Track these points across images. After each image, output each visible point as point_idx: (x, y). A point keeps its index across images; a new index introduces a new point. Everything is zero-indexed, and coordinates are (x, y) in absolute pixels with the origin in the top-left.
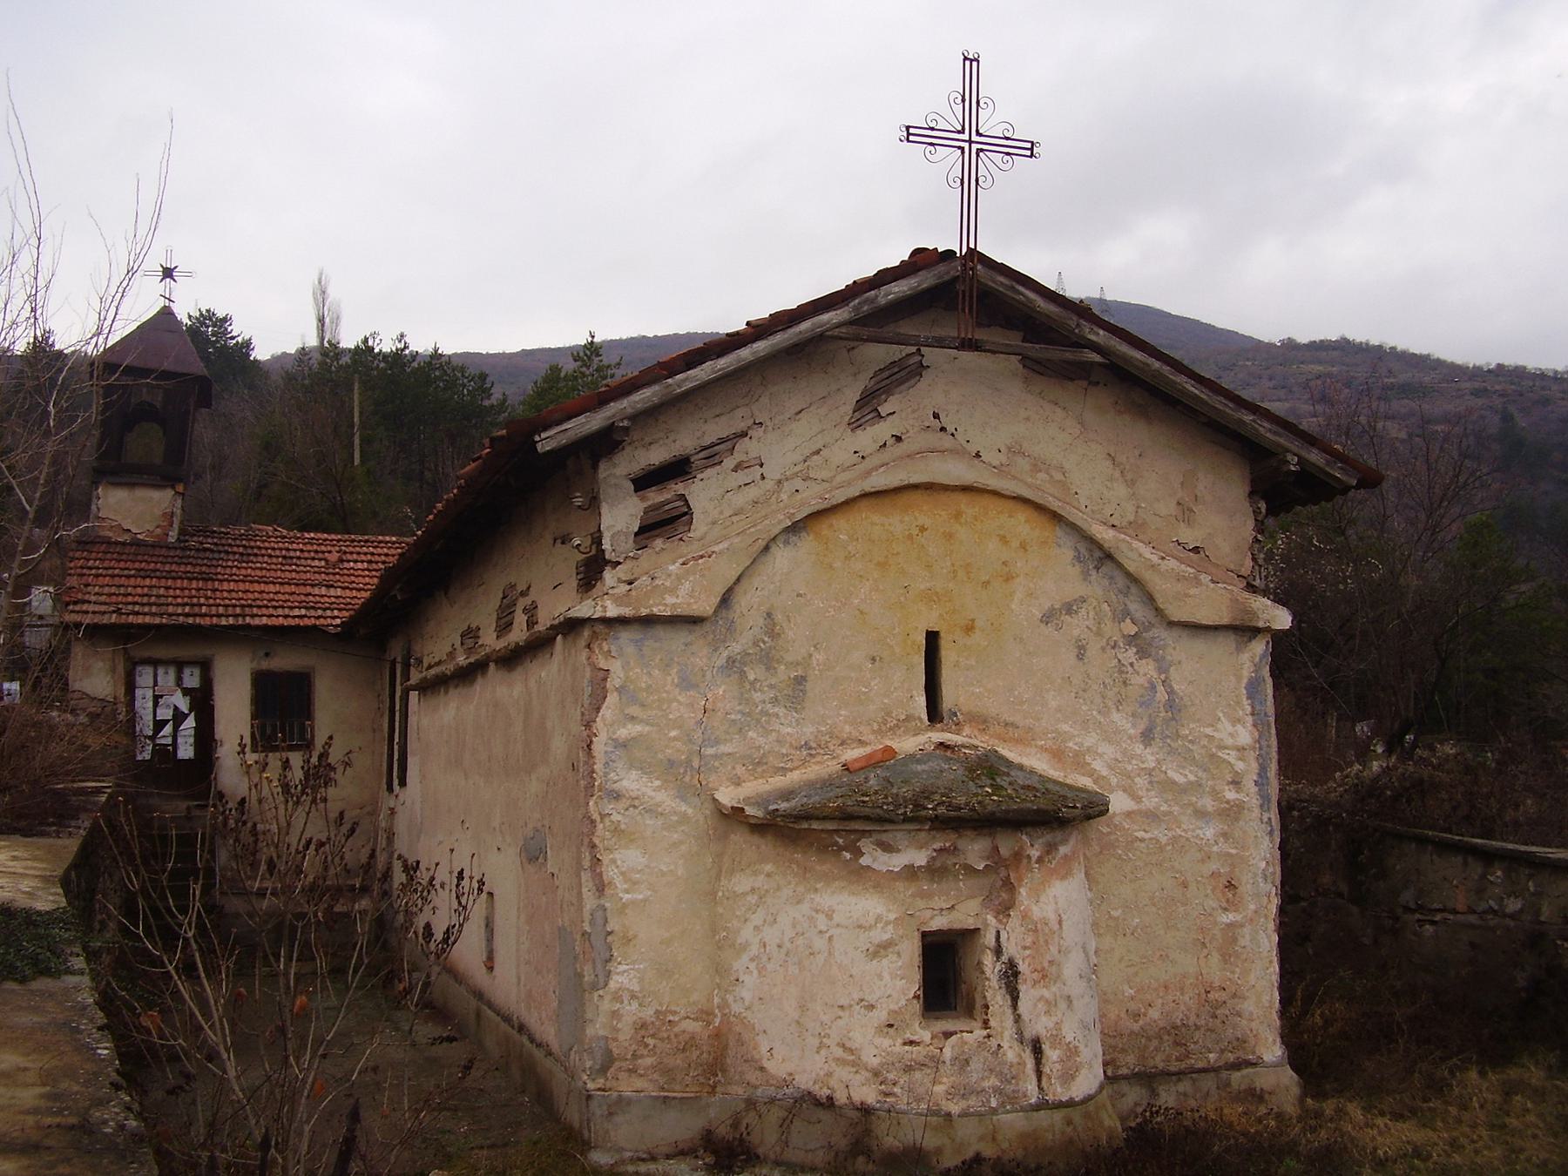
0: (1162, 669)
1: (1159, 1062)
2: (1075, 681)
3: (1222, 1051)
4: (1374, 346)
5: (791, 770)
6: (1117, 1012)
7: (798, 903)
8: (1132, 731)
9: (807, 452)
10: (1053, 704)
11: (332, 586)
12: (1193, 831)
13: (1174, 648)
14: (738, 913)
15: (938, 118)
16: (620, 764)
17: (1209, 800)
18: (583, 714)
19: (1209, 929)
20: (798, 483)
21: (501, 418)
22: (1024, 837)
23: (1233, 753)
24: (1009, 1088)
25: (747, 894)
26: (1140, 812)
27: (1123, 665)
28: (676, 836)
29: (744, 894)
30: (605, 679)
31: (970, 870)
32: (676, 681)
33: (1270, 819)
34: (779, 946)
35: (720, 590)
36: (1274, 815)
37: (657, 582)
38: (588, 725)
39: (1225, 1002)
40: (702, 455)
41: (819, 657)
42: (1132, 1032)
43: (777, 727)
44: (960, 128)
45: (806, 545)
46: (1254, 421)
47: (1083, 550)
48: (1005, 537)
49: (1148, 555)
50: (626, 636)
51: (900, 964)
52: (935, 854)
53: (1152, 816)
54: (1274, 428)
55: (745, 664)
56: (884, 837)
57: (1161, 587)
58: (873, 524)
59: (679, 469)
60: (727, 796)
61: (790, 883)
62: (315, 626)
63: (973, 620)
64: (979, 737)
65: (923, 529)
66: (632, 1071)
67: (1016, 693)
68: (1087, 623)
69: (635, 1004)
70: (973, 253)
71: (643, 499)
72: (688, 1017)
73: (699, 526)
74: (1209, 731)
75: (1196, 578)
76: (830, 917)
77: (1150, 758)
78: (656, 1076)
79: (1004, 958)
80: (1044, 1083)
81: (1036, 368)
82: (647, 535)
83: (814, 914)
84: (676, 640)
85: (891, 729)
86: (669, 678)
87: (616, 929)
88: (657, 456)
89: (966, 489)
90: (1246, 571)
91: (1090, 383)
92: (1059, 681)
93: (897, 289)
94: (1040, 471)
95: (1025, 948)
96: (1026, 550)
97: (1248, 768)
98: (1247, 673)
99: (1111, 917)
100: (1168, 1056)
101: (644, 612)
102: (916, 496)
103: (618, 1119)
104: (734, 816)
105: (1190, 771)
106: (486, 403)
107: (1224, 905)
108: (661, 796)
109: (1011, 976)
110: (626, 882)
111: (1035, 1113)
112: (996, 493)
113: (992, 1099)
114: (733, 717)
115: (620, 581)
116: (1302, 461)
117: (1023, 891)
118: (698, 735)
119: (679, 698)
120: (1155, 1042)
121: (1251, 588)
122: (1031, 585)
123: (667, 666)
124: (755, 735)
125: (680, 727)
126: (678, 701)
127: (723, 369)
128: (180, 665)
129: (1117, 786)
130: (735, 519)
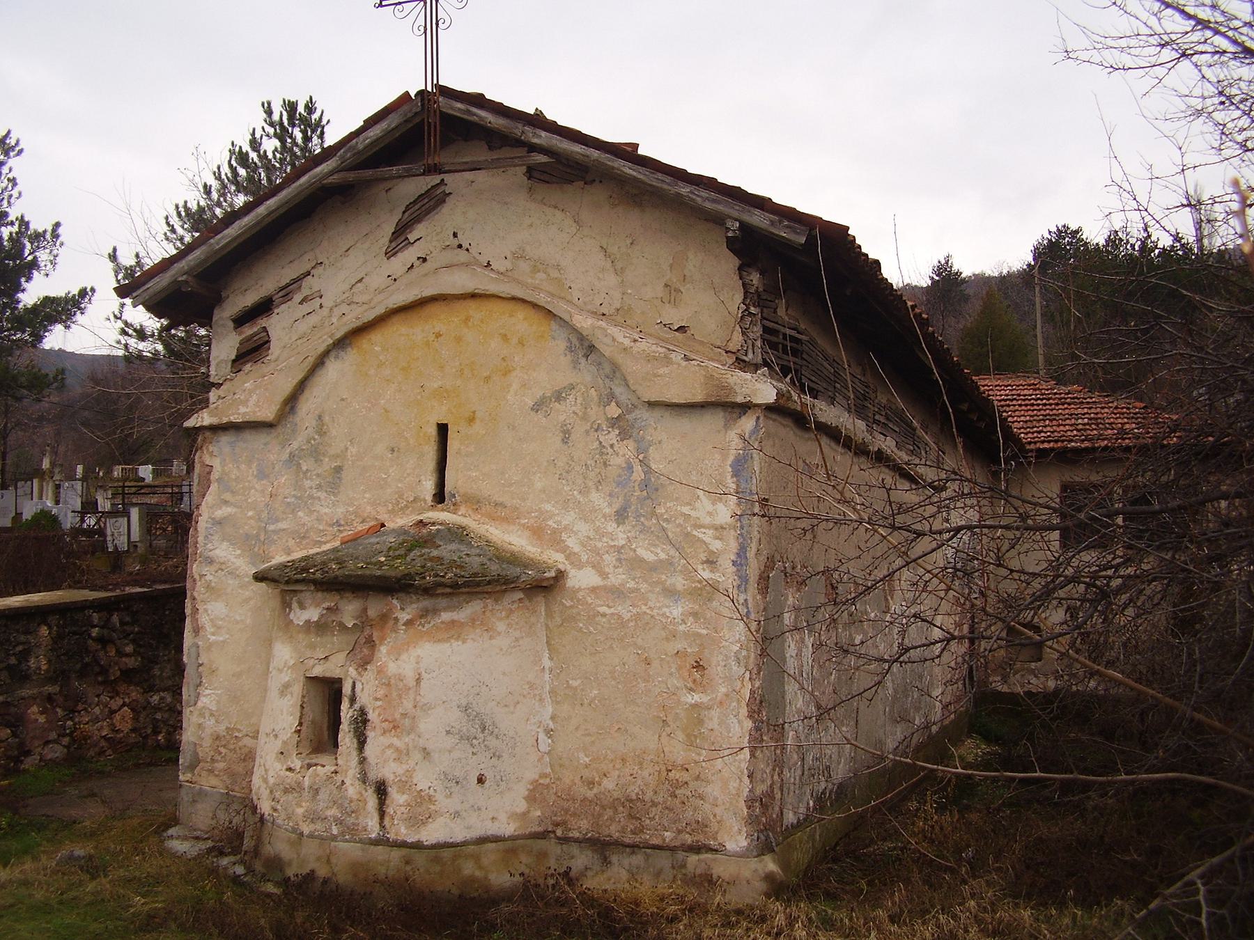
0: (642, 450)
1: (614, 831)
2: (560, 464)
3: (680, 832)
6: (571, 777)
8: (607, 510)
10: (539, 485)
12: (660, 608)
13: (656, 429)
16: (216, 537)
17: (680, 579)
19: (671, 708)
20: (344, 308)
22: (395, 601)
23: (710, 532)
24: (350, 820)
26: (605, 588)
27: (604, 447)
28: (247, 593)
30: (209, 473)
31: (342, 626)
32: (255, 473)
33: (746, 600)
37: (237, 396)
39: (686, 783)
40: (280, 294)
41: (353, 450)
42: (585, 799)
43: (318, 508)
46: (691, 192)
48: (505, 335)
49: (621, 339)
50: (225, 439)
52: (325, 612)
53: (617, 593)
55: (300, 458)
59: (264, 307)
64: (472, 516)
65: (438, 335)
66: (211, 771)
67: (507, 476)
68: (573, 408)
69: (213, 721)
72: (247, 735)
73: (275, 349)
74: (686, 510)
75: (666, 357)
77: (621, 535)
78: (225, 778)
79: (357, 706)
80: (387, 822)
82: (242, 361)
84: (256, 441)
85: (402, 509)
86: (251, 471)
87: (205, 662)
88: (250, 299)
90: (733, 346)
92: (545, 464)
93: (372, 134)
94: (539, 271)
95: (377, 699)
96: (523, 345)
97: (727, 548)
99: (569, 687)
100: (623, 828)
101: (225, 420)
103: (199, 806)
105: (663, 550)
107: (690, 685)
109: (361, 722)
111: (372, 847)
113: (334, 827)
114: (288, 500)
117: (383, 649)
118: (264, 515)
119: (256, 486)
120: (609, 812)
122: (526, 377)
126: (255, 488)
127: (246, 225)
129: (587, 562)
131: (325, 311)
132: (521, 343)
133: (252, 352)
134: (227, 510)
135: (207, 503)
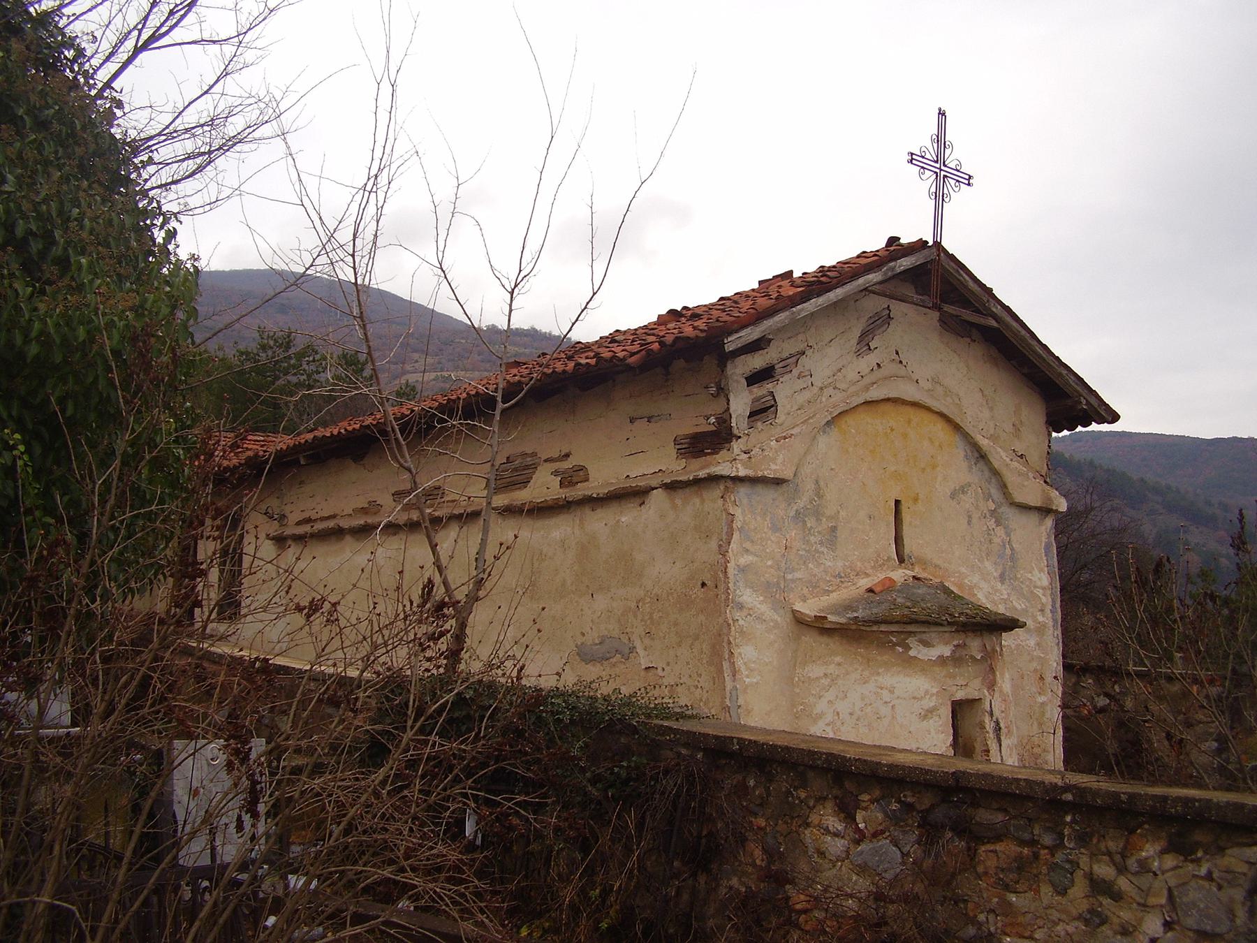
4: (555, 336)
5: (832, 592)
7: (864, 683)
8: (995, 574)
14: (814, 692)
18: (720, 546)
20: (830, 391)
30: (732, 522)
34: (851, 714)
36: (1059, 632)
40: (781, 365)
41: (843, 513)
45: (834, 432)
47: (968, 451)
50: (743, 491)
51: (941, 723)
54: (1076, 381)
56: (924, 637)
57: (1010, 478)
58: (867, 423)
60: (809, 608)
61: (856, 669)
70: (938, 245)
71: (751, 392)
73: (781, 416)
76: (892, 692)
79: (994, 719)
83: (879, 690)
85: (880, 566)
89: (915, 405)
97: (1046, 600)
101: (760, 474)
102: (888, 407)
104: (819, 626)
109: (998, 729)
112: (928, 409)
114: (800, 552)
116: (1088, 403)
124: (812, 566)
130: (799, 411)
131: (815, 390)
132: (940, 446)
135: (732, 551)
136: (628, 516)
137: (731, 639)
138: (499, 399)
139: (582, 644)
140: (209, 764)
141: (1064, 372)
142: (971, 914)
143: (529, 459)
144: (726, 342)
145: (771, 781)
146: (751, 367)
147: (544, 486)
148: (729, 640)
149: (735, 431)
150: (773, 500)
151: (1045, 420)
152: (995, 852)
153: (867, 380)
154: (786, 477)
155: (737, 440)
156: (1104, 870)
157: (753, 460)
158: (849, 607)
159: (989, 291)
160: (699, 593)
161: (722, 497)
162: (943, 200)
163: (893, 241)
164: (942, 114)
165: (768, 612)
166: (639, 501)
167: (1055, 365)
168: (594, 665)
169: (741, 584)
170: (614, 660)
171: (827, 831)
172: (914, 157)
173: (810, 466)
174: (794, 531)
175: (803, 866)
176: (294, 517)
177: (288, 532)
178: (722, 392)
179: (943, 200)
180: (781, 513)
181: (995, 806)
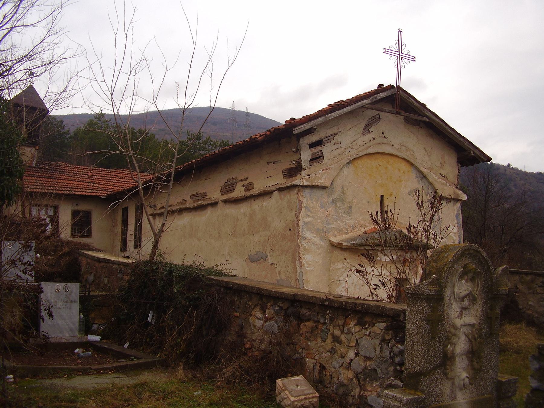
5: (349, 233)
9: (352, 141)
11: (94, 183)
14: (338, 274)
15: (392, 47)
18: (296, 214)
20: (350, 150)
21: (67, 136)
23: (453, 234)
25: (341, 268)
28: (320, 251)
29: (340, 269)
30: (302, 204)
34: (352, 283)
35: (332, 179)
38: (297, 217)
40: (326, 139)
41: (355, 201)
43: (345, 220)
44: (397, 51)
45: (352, 167)
47: (418, 175)
49: (435, 177)
50: (307, 191)
55: (337, 202)
58: (368, 163)
59: (319, 143)
62: (96, 196)
63: (392, 193)
70: (399, 87)
71: (311, 151)
81: (408, 121)
82: (312, 162)
84: (319, 193)
91: (420, 127)
98: (456, 212)
101: (314, 184)
102: (378, 156)
104: (339, 247)
106: (63, 131)
108: (316, 239)
110: (307, 264)
112: (398, 157)
114: (334, 217)
115: (306, 175)
116: (474, 153)
121: (457, 188)
122: (406, 184)
123: (317, 201)
124: (339, 223)
125: (320, 219)
128: (46, 206)
130: (334, 159)
132: (404, 172)
133: (316, 159)
134: (309, 219)
135: (301, 216)
136: (266, 202)
137: (300, 252)
138: (176, 154)
139: (250, 255)
140: (56, 292)
141: (462, 140)
142: (297, 350)
143: (235, 180)
144: (294, 130)
145: (241, 298)
146: (311, 140)
147: (239, 191)
148: (299, 252)
149: (303, 167)
150: (322, 195)
151: (456, 160)
152: (305, 325)
153: (368, 145)
154: (327, 186)
155: (304, 170)
156: (337, 332)
157: (311, 178)
158: (354, 239)
159: (424, 106)
160: (288, 232)
161: (297, 194)
162: (401, 67)
163: (380, 86)
164: (400, 31)
165: (318, 241)
166: (269, 196)
167: (458, 137)
168: (254, 263)
169: (305, 229)
170: (261, 261)
171: (257, 318)
172: (386, 50)
173: (340, 181)
174: (331, 208)
175: (249, 332)
176: (159, 206)
177: (155, 212)
178: (298, 151)
179: (401, 67)
180: (325, 200)
181: (307, 307)
